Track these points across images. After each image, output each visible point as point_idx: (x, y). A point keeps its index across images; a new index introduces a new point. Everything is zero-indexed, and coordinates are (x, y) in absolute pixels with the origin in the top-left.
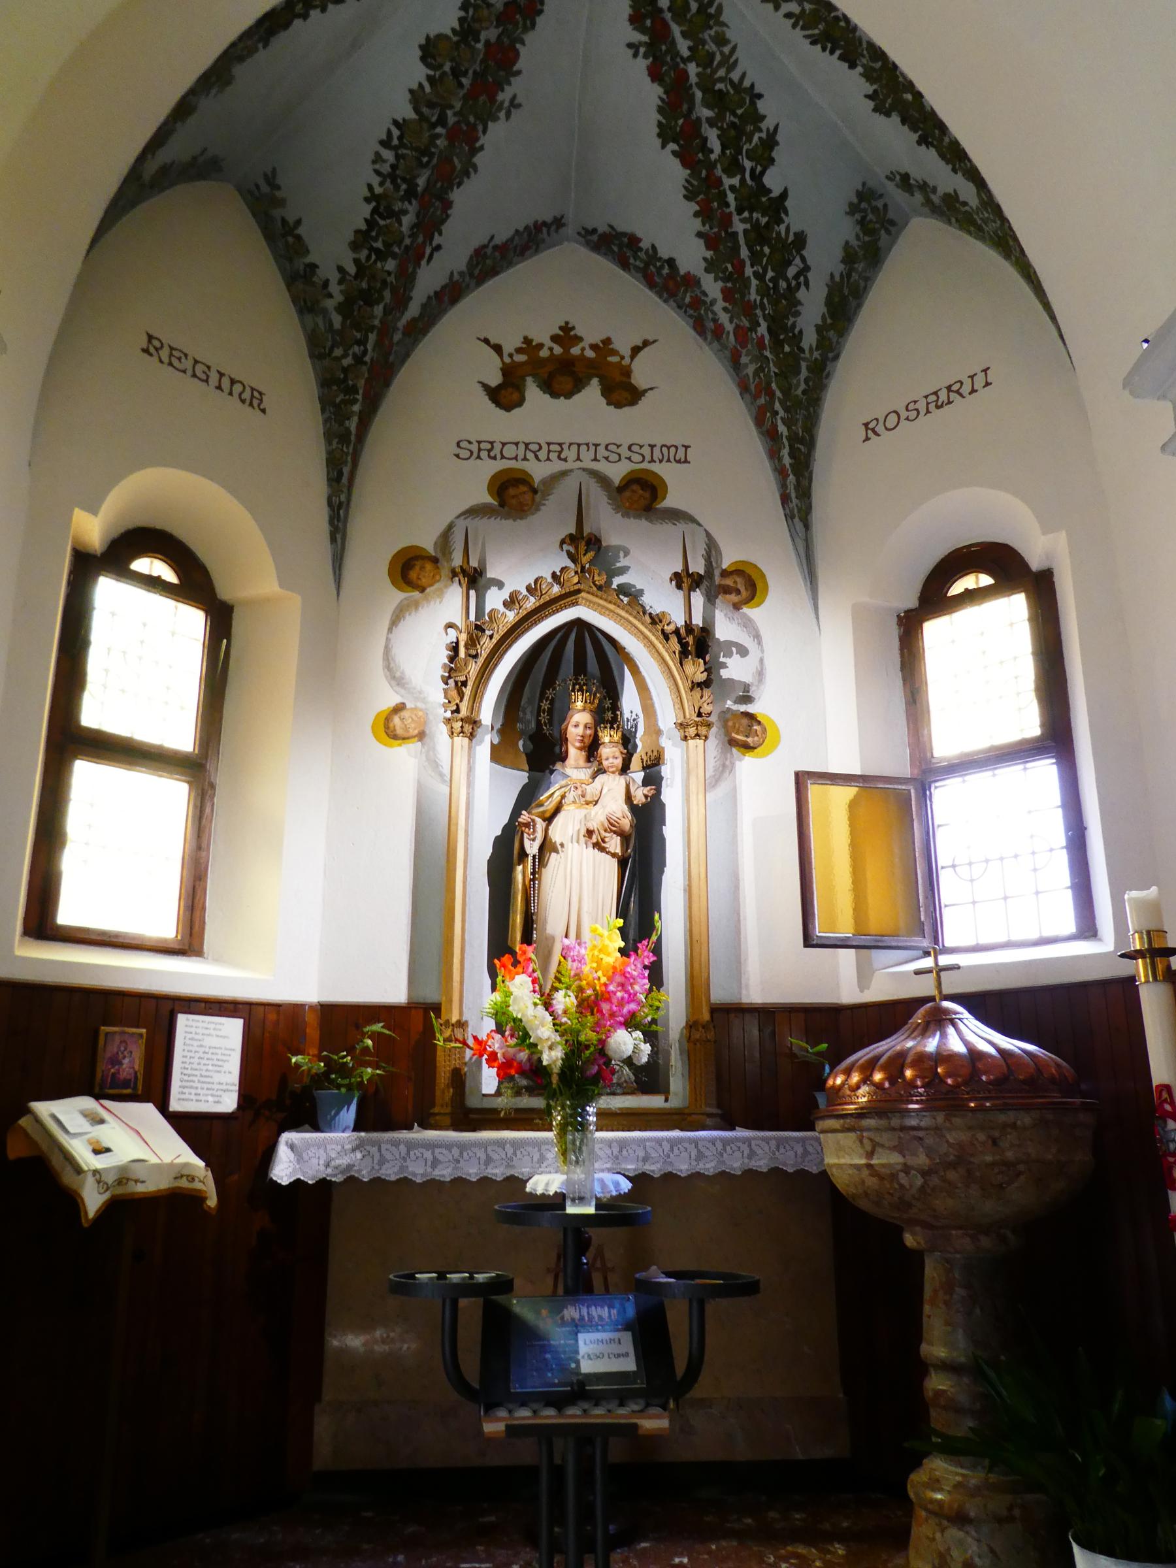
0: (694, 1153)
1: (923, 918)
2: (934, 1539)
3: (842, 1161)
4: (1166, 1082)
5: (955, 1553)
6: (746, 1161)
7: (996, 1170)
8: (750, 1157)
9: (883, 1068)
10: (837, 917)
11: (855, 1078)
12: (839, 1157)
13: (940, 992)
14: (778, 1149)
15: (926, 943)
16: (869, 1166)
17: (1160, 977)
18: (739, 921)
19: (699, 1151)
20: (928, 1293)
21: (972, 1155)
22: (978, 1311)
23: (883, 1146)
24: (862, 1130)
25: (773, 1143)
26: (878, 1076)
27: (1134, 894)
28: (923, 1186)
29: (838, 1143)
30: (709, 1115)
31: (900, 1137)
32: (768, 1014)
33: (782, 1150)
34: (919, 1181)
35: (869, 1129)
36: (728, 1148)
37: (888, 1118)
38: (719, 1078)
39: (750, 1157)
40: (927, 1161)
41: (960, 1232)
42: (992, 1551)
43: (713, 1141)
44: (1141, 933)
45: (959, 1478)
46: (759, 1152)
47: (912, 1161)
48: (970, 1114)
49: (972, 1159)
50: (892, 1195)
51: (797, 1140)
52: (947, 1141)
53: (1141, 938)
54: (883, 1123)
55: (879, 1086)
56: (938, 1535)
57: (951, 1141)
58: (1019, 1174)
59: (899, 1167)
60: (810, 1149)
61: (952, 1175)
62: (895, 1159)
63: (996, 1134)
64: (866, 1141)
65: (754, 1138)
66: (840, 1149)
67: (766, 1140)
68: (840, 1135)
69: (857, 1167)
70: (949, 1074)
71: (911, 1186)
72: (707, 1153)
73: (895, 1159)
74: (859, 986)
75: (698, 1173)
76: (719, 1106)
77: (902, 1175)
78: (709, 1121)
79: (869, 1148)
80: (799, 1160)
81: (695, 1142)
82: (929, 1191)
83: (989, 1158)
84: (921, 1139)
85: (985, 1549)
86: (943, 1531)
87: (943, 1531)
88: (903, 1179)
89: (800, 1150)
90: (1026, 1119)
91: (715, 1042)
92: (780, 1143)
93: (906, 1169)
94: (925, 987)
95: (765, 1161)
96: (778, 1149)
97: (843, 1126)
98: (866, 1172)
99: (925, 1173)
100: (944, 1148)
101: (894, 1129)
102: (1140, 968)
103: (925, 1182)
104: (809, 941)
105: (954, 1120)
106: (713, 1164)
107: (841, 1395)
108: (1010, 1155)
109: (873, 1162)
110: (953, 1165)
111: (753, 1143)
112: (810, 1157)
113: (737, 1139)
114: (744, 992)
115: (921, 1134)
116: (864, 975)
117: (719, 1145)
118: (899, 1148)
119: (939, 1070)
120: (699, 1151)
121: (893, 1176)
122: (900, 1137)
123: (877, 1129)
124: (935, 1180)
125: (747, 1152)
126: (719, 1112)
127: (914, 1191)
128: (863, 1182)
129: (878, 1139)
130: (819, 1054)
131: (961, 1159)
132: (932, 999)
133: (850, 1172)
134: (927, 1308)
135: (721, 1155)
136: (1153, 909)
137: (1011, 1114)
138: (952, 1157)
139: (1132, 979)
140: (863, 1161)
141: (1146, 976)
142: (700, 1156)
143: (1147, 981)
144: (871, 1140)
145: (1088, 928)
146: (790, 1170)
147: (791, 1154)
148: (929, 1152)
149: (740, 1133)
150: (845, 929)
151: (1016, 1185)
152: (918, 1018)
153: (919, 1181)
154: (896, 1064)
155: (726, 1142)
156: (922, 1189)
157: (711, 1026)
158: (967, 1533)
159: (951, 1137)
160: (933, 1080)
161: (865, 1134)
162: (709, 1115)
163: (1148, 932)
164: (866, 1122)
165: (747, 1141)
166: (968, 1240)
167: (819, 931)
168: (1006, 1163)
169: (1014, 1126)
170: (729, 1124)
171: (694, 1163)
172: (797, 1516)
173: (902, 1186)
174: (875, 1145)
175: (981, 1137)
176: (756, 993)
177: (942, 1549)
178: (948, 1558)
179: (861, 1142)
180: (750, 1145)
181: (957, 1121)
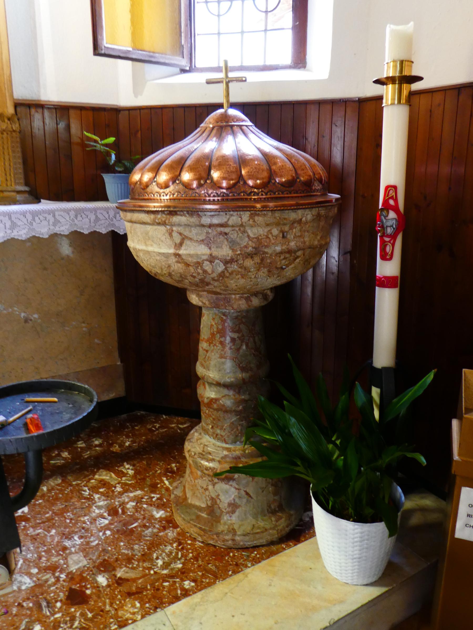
0: (8, 224)
1: (183, 42)
2: (207, 489)
3: (150, 249)
4: (392, 183)
5: (222, 497)
6: (52, 227)
7: (282, 257)
8: (54, 225)
9: (191, 169)
10: (117, 35)
11: (163, 177)
12: (146, 245)
13: (228, 101)
14: (76, 217)
15: (184, 63)
16: (177, 255)
17: (403, 101)
18: (35, 27)
19: (12, 222)
20: (205, 333)
21: (266, 247)
22: (244, 347)
23: (191, 239)
24: (172, 225)
25: (72, 214)
26: (186, 176)
27: (392, 26)
28: (223, 272)
29: (147, 233)
30: (19, 192)
31: (208, 233)
32: (63, 110)
33: (79, 218)
34: (221, 268)
35: (179, 225)
36: (37, 218)
37: (199, 216)
38: (25, 162)
39: (54, 225)
40: (230, 252)
41: (238, 296)
42: (247, 494)
43: (24, 214)
44: (394, 61)
45: (225, 453)
46: (62, 220)
47: (216, 252)
48: (270, 213)
49: (266, 250)
50: (194, 277)
51: (91, 210)
52: (248, 236)
53: (395, 66)
54: (194, 220)
55: (187, 186)
56: (210, 487)
57: (252, 235)
58: (298, 257)
59: (205, 257)
60: (100, 216)
61: (249, 263)
62: (203, 250)
63: (286, 228)
64: (175, 234)
65: (58, 210)
66: (147, 238)
67: (67, 211)
68: (149, 228)
69: (166, 256)
70: (251, 177)
71: (213, 272)
72: (19, 223)
73: (203, 250)
74: (134, 92)
75: (13, 239)
76: (27, 184)
77: (207, 263)
78: (19, 197)
79: (178, 240)
80: (93, 224)
81: (9, 215)
82: (227, 275)
83: (278, 249)
84: (226, 234)
85: (243, 493)
86: (214, 485)
87: (214, 485)
88: (207, 267)
89: (93, 217)
90: (308, 215)
91: (20, 132)
92: (78, 212)
93: (212, 259)
94: (214, 95)
95: (67, 227)
96: (76, 217)
97: (154, 220)
98: (173, 260)
99: (226, 262)
100: (245, 241)
101: (203, 226)
102: (388, 92)
103: (226, 269)
104: (97, 50)
105: (256, 218)
106: (25, 231)
107: (119, 363)
108: (292, 244)
109: (181, 252)
110: (251, 256)
111: (57, 214)
112: (100, 222)
113: (44, 212)
114: (42, 91)
115: (227, 230)
116: (138, 84)
117: (29, 217)
118: (207, 242)
119: (243, 172)
120: (12, 222)
121: (199, 264)
122: (208, 233)
123: (187, 225)
124: (234, 267)
125: (52, 220)
126: (27, 189)
127: (215, 275)
128: (169, 266)
129: (186, 233)
130: (106, 145)
131: (257, 252)
132: (220, 106)
133: (158, 258)
134: (203, 345)
135: (31, 224)
136: (408, 41)
137: (300, 212)
138: (250, 248)
139: (379, 99)
140: (172, 251)
141: (393, 99)
142: (14, 226)
143: (393, 104)
144: (180, 234)
145: (300, 60)
146: (86, 232)
147: (87, 220)
148: (233, 244)
149: (45, 205)
150: (123, 44)
151: (293, 266)
152: (210, 120)
153: (221, 268)
154: (203, 167)
155: (35, 214)
156: (222, 275)
157: (16, 119)
158: (231, 485)
159: (252, 232)
160: (238, 182)
161: (174, 228)
162: (19, 192)
163: (402, 62)
164: (176, 219)
165: (52, 212)
166: (243, 301)
167: (106, 42)
168: (289, 252)
169: (300, 222)
170: (35, 197)
171: (9, 231)
172: (97, 442)
173: (205, 272)
174: (184, 238)
175: (275, 231)
176: (53, 94)
177: (214, 496)
178: (218, 501)
179: (171, 235)
180: (54, 216)
181: (259, 219)
